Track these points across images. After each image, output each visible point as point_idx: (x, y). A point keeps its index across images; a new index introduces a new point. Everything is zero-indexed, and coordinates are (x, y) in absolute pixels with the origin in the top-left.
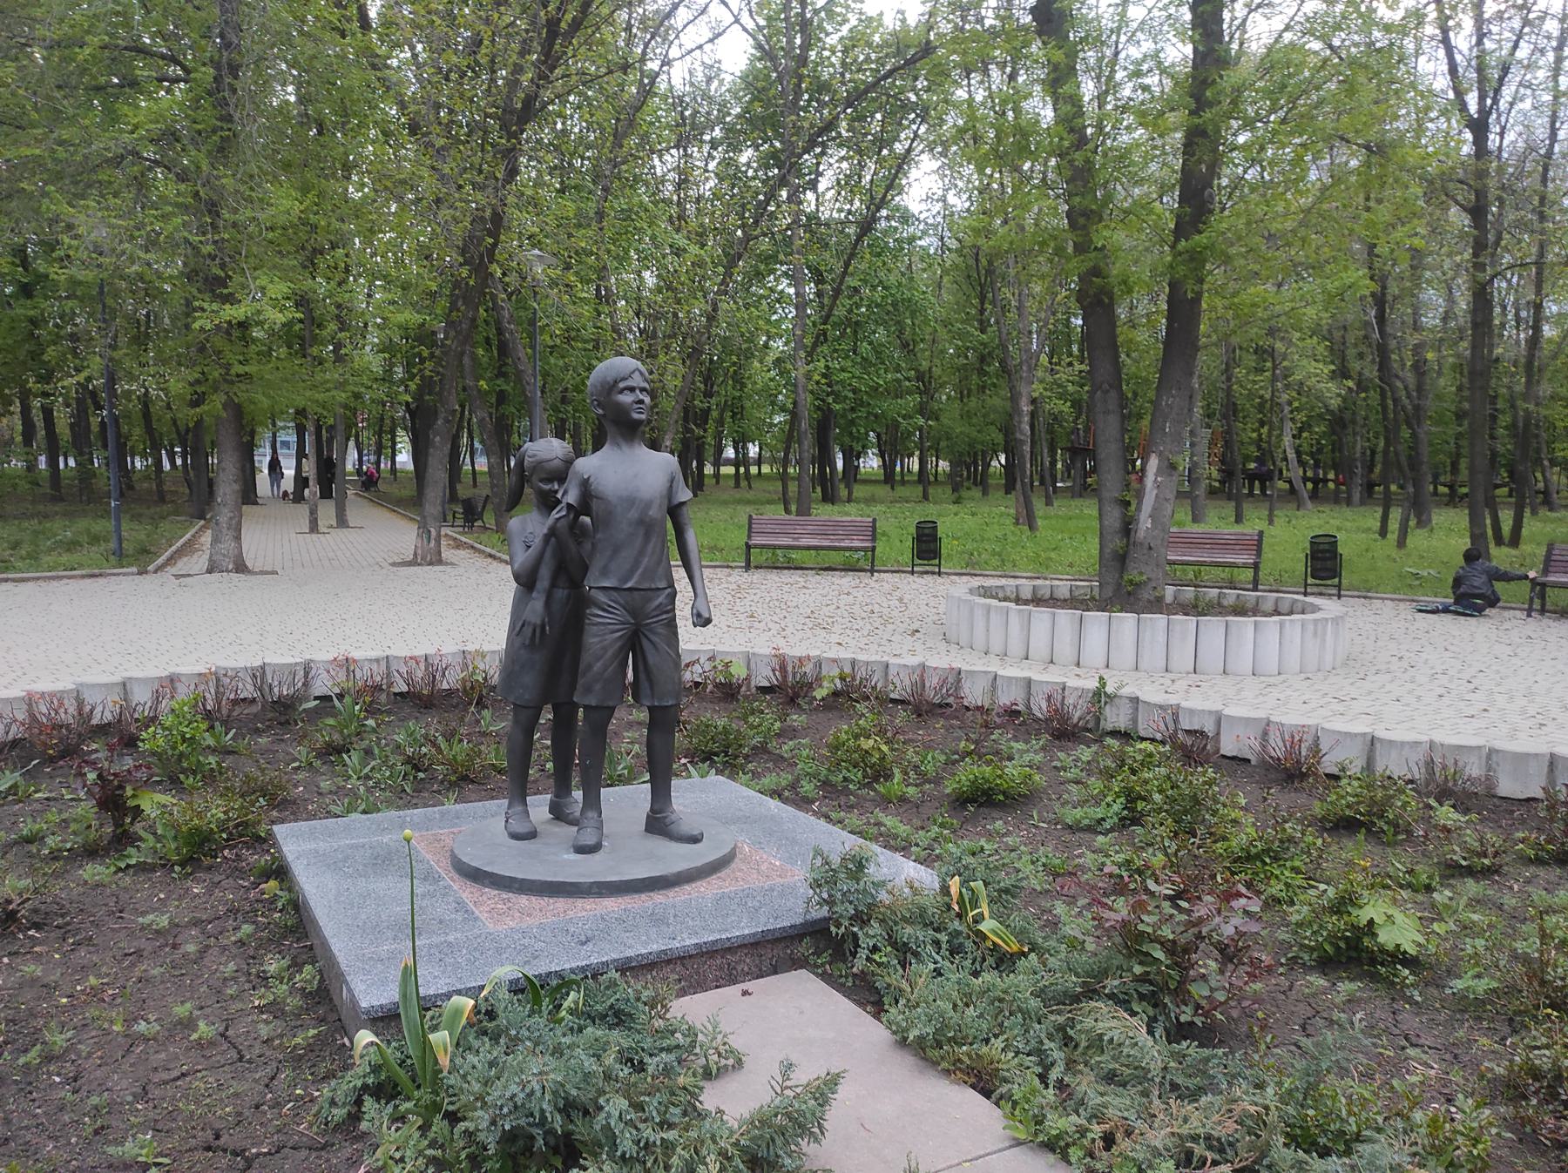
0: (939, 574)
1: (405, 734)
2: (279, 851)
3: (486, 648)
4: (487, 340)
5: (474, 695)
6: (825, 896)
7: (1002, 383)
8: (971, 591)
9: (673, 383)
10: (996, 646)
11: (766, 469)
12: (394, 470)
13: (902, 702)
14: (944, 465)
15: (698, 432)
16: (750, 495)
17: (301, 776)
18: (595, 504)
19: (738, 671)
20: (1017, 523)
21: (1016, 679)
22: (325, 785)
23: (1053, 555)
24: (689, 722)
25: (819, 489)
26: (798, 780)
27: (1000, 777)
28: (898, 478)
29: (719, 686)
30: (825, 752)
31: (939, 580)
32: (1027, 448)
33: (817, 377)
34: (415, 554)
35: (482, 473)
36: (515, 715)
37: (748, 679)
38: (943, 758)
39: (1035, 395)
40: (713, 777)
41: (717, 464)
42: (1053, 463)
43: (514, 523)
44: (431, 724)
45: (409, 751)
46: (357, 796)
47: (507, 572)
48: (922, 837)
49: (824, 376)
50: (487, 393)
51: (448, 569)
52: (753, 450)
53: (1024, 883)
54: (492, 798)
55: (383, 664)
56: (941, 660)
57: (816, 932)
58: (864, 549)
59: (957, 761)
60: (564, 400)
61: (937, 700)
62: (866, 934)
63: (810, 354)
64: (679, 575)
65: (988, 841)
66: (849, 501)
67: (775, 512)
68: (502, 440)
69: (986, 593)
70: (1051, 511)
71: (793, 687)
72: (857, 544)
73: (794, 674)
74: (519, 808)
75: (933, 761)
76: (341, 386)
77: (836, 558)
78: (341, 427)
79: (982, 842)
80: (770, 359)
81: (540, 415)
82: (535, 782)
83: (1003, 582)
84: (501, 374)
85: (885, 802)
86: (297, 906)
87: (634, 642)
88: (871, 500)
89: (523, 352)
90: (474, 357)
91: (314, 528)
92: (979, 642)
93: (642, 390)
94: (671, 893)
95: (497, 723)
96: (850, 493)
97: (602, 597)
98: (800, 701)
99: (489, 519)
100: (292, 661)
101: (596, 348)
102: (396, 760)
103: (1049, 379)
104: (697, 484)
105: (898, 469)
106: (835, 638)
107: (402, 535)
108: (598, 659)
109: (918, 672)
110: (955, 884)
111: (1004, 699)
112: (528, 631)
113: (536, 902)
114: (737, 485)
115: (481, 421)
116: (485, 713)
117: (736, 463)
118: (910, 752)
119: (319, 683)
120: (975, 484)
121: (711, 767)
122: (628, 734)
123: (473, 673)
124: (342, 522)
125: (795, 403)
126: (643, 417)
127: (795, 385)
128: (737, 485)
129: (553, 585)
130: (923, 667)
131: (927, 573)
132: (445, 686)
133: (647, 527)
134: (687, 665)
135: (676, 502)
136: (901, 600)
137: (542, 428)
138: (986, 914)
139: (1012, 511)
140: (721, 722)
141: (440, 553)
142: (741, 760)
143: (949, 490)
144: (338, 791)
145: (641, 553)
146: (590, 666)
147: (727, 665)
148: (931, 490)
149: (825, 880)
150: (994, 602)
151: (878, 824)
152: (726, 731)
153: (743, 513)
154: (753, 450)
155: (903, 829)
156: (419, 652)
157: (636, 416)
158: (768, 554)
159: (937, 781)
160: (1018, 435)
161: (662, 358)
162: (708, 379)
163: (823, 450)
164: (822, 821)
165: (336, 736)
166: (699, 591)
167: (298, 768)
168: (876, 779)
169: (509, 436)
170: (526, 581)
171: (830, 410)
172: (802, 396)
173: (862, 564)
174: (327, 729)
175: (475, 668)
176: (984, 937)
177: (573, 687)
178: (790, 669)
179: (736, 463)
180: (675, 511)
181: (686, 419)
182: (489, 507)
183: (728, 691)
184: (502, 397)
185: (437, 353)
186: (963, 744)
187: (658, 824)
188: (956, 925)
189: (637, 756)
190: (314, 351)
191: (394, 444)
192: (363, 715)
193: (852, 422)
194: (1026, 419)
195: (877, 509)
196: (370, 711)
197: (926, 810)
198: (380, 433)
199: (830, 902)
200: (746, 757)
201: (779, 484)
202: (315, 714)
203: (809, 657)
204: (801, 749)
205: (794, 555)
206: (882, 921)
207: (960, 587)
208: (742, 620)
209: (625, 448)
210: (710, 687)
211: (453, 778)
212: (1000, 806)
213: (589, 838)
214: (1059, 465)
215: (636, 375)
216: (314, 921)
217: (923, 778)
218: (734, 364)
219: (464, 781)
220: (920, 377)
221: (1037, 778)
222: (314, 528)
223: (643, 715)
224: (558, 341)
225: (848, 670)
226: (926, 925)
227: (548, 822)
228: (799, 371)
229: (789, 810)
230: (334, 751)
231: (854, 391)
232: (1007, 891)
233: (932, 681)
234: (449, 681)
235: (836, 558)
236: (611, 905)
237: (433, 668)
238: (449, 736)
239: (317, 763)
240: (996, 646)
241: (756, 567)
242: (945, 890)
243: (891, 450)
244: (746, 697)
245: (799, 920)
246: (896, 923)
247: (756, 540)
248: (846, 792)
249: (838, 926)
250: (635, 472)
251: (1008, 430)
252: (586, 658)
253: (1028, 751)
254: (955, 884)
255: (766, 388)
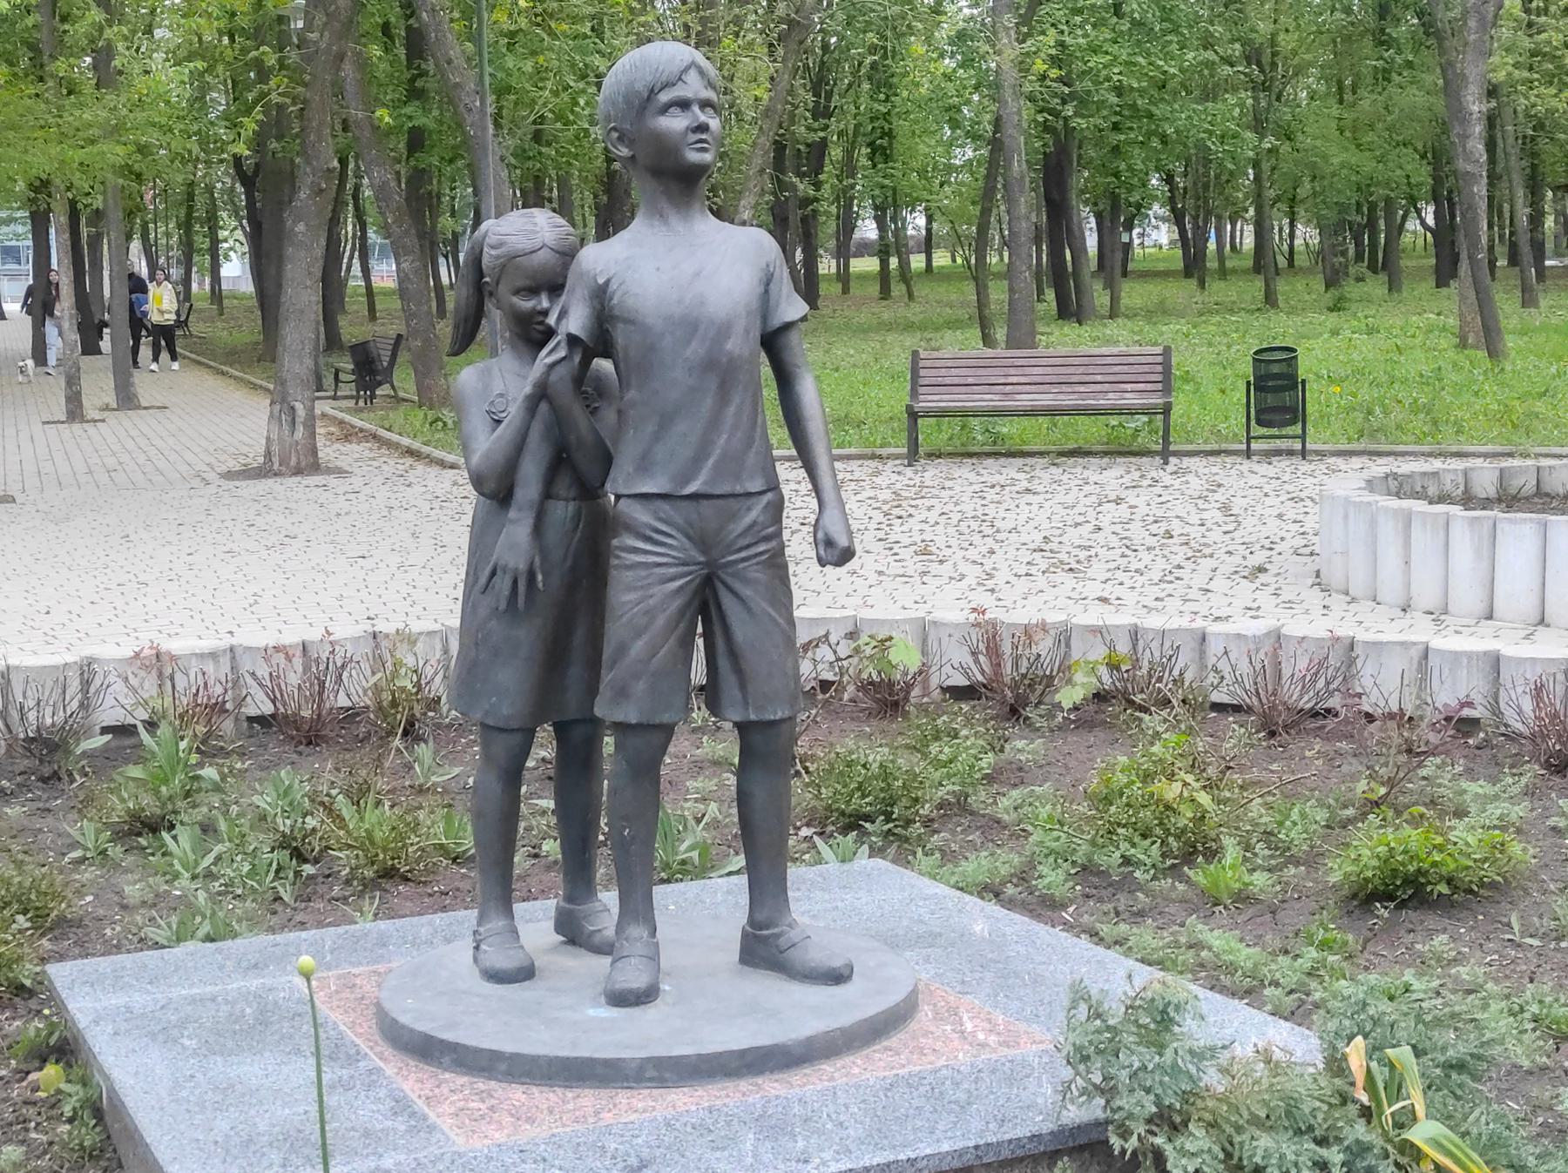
0: (1304, 453)
1: (280, 790)
2: (61, 1008)
3: (416, 626)
4: (386, 28)
5: (400, 720)
6: (1097, 1078)
7: (1429, 57)
8: (1370, 485)
9: (753, 94)
10: (1427, 594)
11: (941, 259)
12: (217, 295)
13: (1237, 709)
14: (1307, 235)
15: (803, 187)
16: (914, 312)
17: (88, 874)
18: (620, 336)
19: (905, 657)
20: (1463, 344)
21: (1469, 655)
22: (133, 891)
23: (1539, 406)
24: (813, 758)
25: (1050, 295)
26: (1031, 864)
27: (1440, 848)
28: (1212, 264)
29: (867, 686)
30: (1083, 808)
31: (1305, 467)
32: (1481, 189)
33: (1039, 66)
34: (268, 454)
35: (386, 293)
36: (486, 746)
37: (923, 671)
38: (1321, 816)
39: (1501, 76)
40: (864, 862)
41: (844, 252)
42: (1536, 219)
43: (468, 376)
44: (321, 774)
45: (284, 825)
46: (193, 910)
47: (463, 476)
48: (1286, 970)
49: (1055, 61)
50: (389, 132)
51: (331, 480)
52: (916, 222)
53: (1496, 1050)
54: (444, 909)
55: (225, 667)
56: (1312, 623)
57: (1081, 1149)
58: (1147, 411)
59: (1350, 821)
60: (537, 137)
61: (1306, 703)
62: (1183, 1152)
63: (1025, 20)
64: (791, 477)
65: (1420, 975)
66: (1113, 314)
67: (964, 344)
68: (421, 217)
69: (1401, 487)
70: (1536, 317)
71: (1015, 686)
72: (1132, 400)
73: (1016, 665)
74: (497, 923)
75: (1303, 822)
76: (115, 131)
77: (1090, 430)
78: (116, 215)
79: (1409, 976)
80: (944, 32)
81: (496, 174)
82: (522, 878)
83: (1437, 464)
84: (415, 93)
85: (1209, 902)
86: (101, 1111)
87: (706, 602)
88: (1158, 312)
89: (457, 49)
90: (363, 64)
91: (75, 411)
92: (1390, 588)
93: (705, 104)
94: (797, 1077)
95: (451, 767)
96: (1114, 300)
97: (641, 515)
98: (1029, 712)
99: (404, 380)
100: (57, 660)
101: (597, 31)
102: (261, 841)
103: (1527, 43)
104: (808, 287)
105: (1212, 245)
106: (1094, 589)
107: (237, 419)
108: (639, 634)
109: (1267, 647)
110: (1356, 1054)
111: (1445, 696)
112: (503, 585)
113: (543, 1097)
114: (885, 292)
115: (381, 192)
116: (424, 751)
117: (883, 251)
118: (1256, 808)
119: (110, 701)
120: (1373, 268)
121: (859, 841)
122: (699, 780)
123: (395, 674)
124: (126, 399)
125: (997, 123)
126: (708, 157)
127: (997, 86)
128: (885, 292)
129: (548, 494)
130: (1277, 637)
131: (1278, 453)
132: (343, 701)
133: (722, 374)
134: (806, 647)
135: (776, 322)
136: (1225, 508)
137: (499, 196)
138: (1420, 1110)
139: (1452, 321)
140: (876, 756)
141: (314, 451)
142: (917, 829)
143: (1318, 284)
144: (157, 901)
145: (714, 424)
146: (622, 649)
147: (884, 643)
148: (1282, 286)
149: (1095, 1047)
150: (1419, 506)
151: (1195, 946)
152: (885, 774)
153: (898, 352)
154: (916, 222)
155: (1246, 955)
156: (291, 638)
157: (693, 157)
158: (951, 427)
159: (1312, 860)
160: (1461, 165)
161: (728, 44)
162: (819, 84)
163: (1066, 207)
164: (1084, 942)
165: (147, 800)
166: (829, 494)
167: (83, 860)
168: (1189, 857)
169: (435, 216)
170: (497, 490)
171: (1069, 131)
172: (1012, 106)
173: (1143, 440)
174: (129, 791)
175: (397, 665)
176: (1417, 1155)
177: (592, 690)
178: (1007, 648)
179: (883, 251)
180: (773, 341)
181: (779, 164)
182: (404, 356)
183: (887, 699)
184: (416, 140)
185: (293, 56)
186: (1362, 785)
187: (763, 948)
188: (1360, 1131)
189: (715, 824)
190: (60, 67)
191: (215, 242)
192: (194, 759)
193: (1116, 150)
194: (1478, 129)
195: (1169, 331)
196: (208, 750)
197: (1292, 917)
198: (186, 225)
199: (1108, 1090)
200: (928, 822)
201: (969, 289)
202: (105, 761)
203: (1043, 627)
204: (1035, 803)
205: (1006, 427)
206: (1212, 1125)
207: (1347, 480)
208: (906, 562)
209: (674, 220)
210: (851, 688)
211: (369, 873)
212: (1444, 905)
213: (633, 976)
214: (1549, 222)
215: (692, 77)
216: (133, 1135)
217: (1285, 855)
218: (873, 49)
219: (389, 877)
220: (1252, 56)
221: (1516, 848)
222: (75, 411)
223: (728, 747)
224: (523, 23)
225: (1123, 648)
226: (1299, 1132)
227: (554, 949)
228: (1003, 56)
229: (1016, 924)
230: (145, 827)
231: (1119, 90)
232: (1460, 1066)
233: (1296, 665)
234: (353, 692)
235: (1090, 430)
236: (684, 1101)
237: (321, 667)
238: (357, 796)
239: (115, 851)
240: (1427, 594)
241: (931, 456)
242: (1337, 1065)
243: (1194, 210)
244: (923, 709)
245: (1047, 1127)
246: (1239, 1129)
247: (928, 401)
248: (1128, 884)
249: (1125, 1134)
250: (693, 268)
251: (1439, 157)
252: (615, 631)
253: (1496, 797)
254: (1356, 1054)
255: (937, 95)
